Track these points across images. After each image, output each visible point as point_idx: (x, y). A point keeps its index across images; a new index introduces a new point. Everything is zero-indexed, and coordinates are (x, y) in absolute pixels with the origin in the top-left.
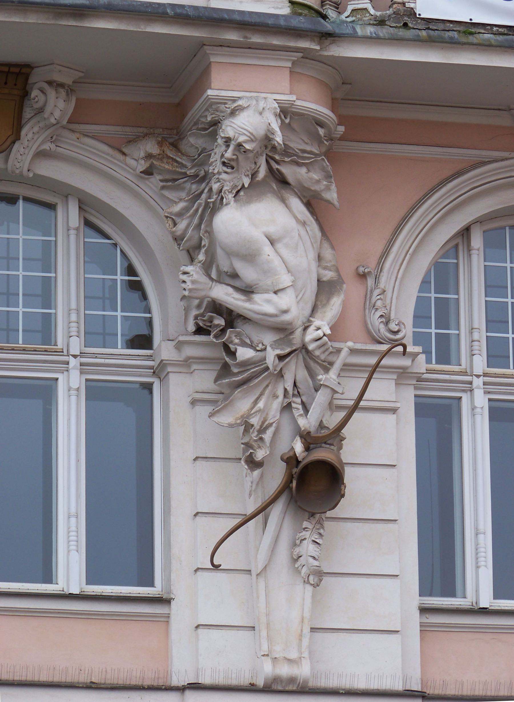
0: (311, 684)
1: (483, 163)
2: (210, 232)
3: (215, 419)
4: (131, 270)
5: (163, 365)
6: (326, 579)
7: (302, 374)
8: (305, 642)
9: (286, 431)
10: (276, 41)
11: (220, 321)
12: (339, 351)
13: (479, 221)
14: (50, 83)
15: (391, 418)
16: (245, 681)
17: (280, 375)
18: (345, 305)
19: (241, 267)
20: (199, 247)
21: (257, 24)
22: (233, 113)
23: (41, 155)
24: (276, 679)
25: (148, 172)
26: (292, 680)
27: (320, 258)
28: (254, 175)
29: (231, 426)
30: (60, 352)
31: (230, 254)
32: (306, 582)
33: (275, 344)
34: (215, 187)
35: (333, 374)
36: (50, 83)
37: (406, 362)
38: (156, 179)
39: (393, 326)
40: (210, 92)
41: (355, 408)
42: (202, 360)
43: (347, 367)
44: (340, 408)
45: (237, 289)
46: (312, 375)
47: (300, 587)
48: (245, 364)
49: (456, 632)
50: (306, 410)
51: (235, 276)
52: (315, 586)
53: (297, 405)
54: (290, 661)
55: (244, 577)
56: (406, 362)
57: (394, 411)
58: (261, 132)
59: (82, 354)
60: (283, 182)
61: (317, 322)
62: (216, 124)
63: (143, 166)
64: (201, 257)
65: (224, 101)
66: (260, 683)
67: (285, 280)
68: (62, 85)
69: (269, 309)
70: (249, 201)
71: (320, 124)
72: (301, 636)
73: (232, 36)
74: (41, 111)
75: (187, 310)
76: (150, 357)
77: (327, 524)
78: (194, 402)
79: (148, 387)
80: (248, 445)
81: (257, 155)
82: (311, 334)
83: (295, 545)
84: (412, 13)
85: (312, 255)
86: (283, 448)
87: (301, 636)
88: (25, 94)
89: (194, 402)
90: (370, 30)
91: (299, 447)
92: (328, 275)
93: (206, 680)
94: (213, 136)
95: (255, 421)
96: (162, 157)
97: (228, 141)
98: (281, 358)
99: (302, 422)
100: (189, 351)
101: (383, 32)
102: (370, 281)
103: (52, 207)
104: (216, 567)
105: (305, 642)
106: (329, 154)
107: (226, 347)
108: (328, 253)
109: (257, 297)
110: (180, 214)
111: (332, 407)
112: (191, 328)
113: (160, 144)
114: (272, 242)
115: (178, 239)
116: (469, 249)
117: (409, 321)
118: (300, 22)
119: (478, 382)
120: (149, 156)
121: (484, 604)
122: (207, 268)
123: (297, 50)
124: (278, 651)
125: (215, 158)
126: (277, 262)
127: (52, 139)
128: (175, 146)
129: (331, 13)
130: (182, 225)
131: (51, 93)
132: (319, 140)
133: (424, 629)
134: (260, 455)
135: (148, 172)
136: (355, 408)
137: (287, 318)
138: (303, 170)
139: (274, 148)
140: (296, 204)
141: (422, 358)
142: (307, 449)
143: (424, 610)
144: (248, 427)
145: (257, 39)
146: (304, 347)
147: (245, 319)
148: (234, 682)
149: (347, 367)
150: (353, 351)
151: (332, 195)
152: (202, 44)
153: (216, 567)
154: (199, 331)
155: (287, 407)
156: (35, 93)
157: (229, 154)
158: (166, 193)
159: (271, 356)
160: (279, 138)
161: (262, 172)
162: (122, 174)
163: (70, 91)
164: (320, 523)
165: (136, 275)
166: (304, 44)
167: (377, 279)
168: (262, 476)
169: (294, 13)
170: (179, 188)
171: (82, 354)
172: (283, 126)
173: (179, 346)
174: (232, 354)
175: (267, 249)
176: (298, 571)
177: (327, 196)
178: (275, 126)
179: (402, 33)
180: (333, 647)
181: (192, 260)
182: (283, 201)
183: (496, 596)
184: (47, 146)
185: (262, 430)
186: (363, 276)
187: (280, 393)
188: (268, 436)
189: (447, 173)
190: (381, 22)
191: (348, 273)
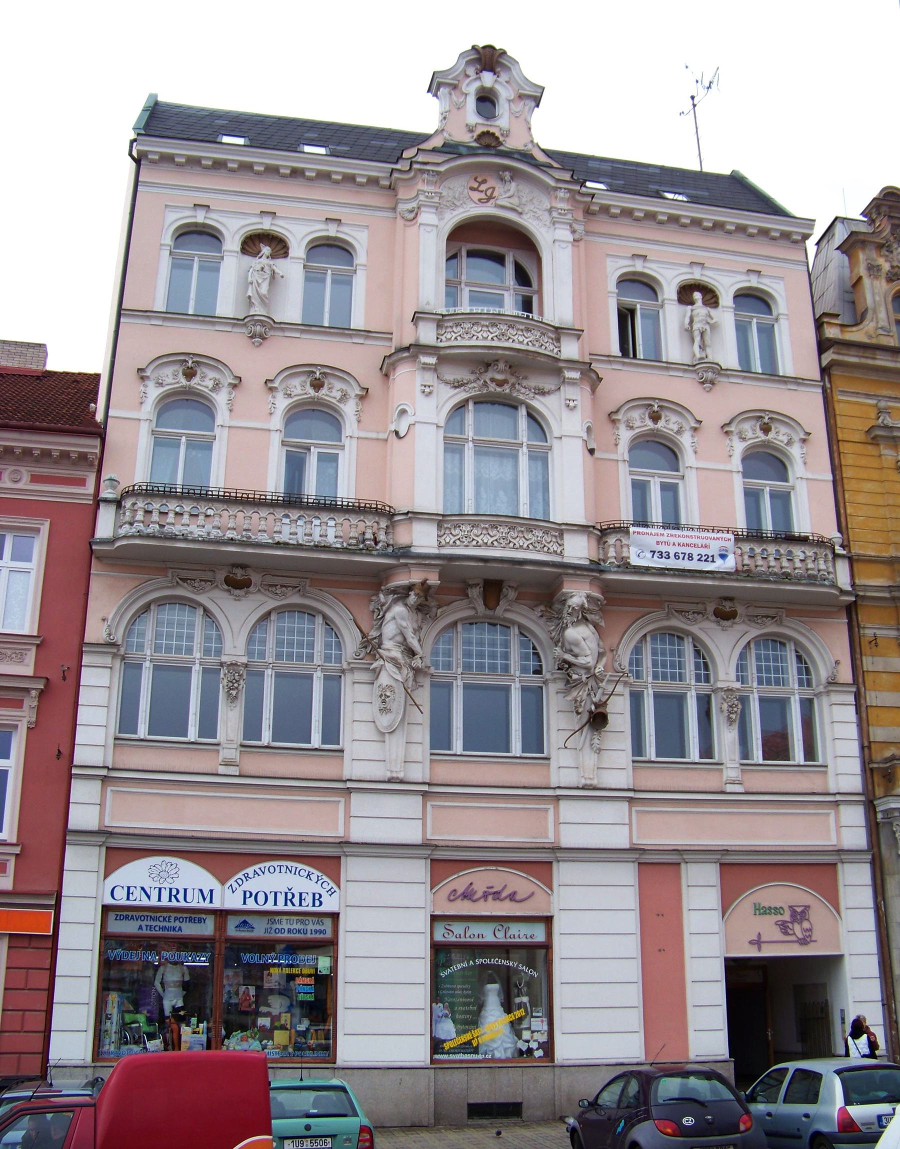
0: (598, 786)
1: (650, 613)
2: (563, 636)
3: (566, 698)
4: (534, 648)
5: (547, 680)
6: (602, 752)
7: (594, 683)
8: (595, 772)
9: (589, 702)
10: (585, 573)
11: (566, 666)
12: (606, 676)
13: (649, 632)
14: (509, 586)
15: (622, 698)
16: (576, 786)
17: (587, 684)
18: (607, 660)
19: (574, 648)
20: (559, 641)
21: (550, 950)
22: (571, 597)
23: (506, 610)
24: (586, 785)
25: (542, 616)
26: (591, 785)
27: (598, 645)
28: (578, 617)
29: (571, 701)
30: (512, 676)
31: (570, 644)
32: (595, 752)
33: (585, 674)
34: (565, 621)
35: (604, 683)
36: (509, 586)
37: (627, 679)
38: (544, 618)
39: (622, 667)
40: (564, 590)
41: (612, 694)
42: (559, 678)
43: (609, 681)
44: (607, 694)
45: (573, 655)
46: (597, 684)
47: (593, 754)
48: (575, 680)
49: (775, 944)
50: (595, 695)
51: (571, 651)
52: (598, 753)
53: (592, 694)
54: (590, 779)
55: (575, 751)
56: (627, 679)
57: (623, 695)
58: (580, 604)
59: (520, 677)
60: (587, 620)
61: (599, 666)
62: (565, 600)
63: (540, 614)
64: (560, 644)
65: (568, 593)
66: (581, 786)
67: (588, 652)
68: (513, 587)
69: (583, 662)
70: (577, 626)
71: (599, 600)
72: (594, 771)
73: (571, 571)
74: (506, 596)
75: (555, 663)
76: (542, 678)
77: (603, 733)
78: (557, 693)
79: (541, 688)
80: (576, 707)
81: (579, 611)
82: (597, 670)
83: (591, 740)
84: (629, 563)
85: (596, 644)
86: (588, 708)
87: (594, 771)
88: (501, 590)
89: (557, 693)
90: (616, 569)
91: (593, 708)
92: (601, 650)
93: (562, 785)
94: (564, 604)
95: (579, 699)
96: (547, 611)
97: (569, 606)
98: (587, 678)
99: (594, 699)
100: (556, 676)
101: (620, 570)
102: (614, 652)
103: (509, 628)
104: (566, 748)
105: (595, 772)
106: (600, 610)
107: (568, 674)
108: (601, 643)
109: (579, 658)
110: (553, 630)
111: (604, 694)
112: (557, 668)
113: (546, 607)
114: (584, 640)
115: (552, 639)
116: (646, 641)
117: (627, 665)
118: (592, 567)
119: (650, 685)
120: (542, 611)
121: (653, 759)
122: (562, 647)
123: (592, 576)
124: (586, 775)
125: (565, 612)
126: (586, 647)
127: (509, 605)
128: (550, 607)
129: (602, 563)
130: (554, 634)
131: (510, 590)
132: (598, 605)
133: (634, 768)
134: (580, 710)
135: (542, 616)
136: (612, 694)
137: (589, 665)
138: (593, 616)
139: (585, 609)
140: (591, 627)
141: (632, 678)
142: (596, 708)
143: (634, 762)
144: (576, 701)
145: (579, 572)
146: (595, 675)
147: (575, 665)
148: (572, 786)
149: (609, 681)
150: (611, 676)
151: (603, 624)
152: (561, 574)
153: (566, 748)
154: (559, 669)
155: (589, 695)
156: (504, 590)
157: (570, 611)
158: (548, 623)
159: (584, 678)
160: (586, 606)
161: (580, 617)
162: (534, 618)
163: (516, 589)
164: (600, 733)
165: (536, 650)
166: (594, 574)
167: (617, 651)
168: (581, 717)
169: (591, 564)
170: (552, 622)
171: (520, 677)
172: (588, 601)
173: (552, 674)
174: (571, 677)
175: (583, 643)
176: (593, 749)
177: (601, 624)
178: (585, 601)
179: (626, 570)
180: (660, 950)
181: (556, 646)
182: (587, 626)
183: (657, 756)
184: (508, 607)
185: (581, 702)
186: (612, 651)
187: (587, 690)
188: (583, 704)
189: (640, 616)
190: (619, 566)
191: (607, 649)
